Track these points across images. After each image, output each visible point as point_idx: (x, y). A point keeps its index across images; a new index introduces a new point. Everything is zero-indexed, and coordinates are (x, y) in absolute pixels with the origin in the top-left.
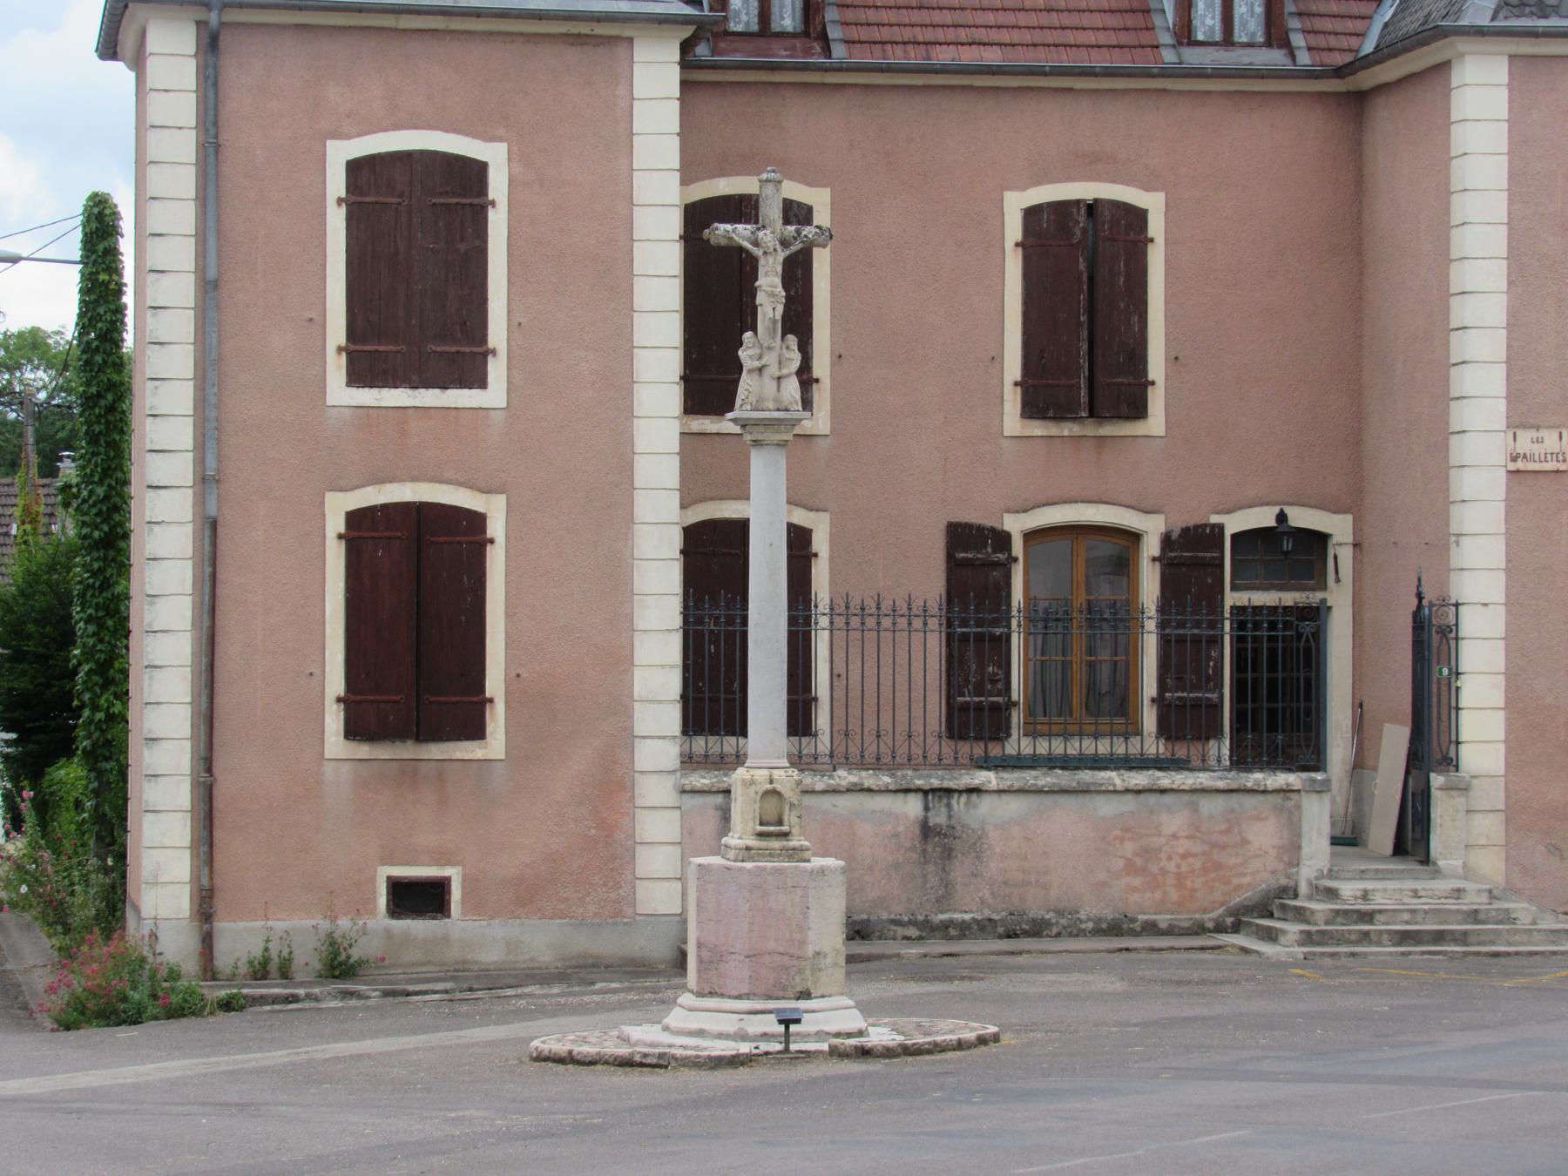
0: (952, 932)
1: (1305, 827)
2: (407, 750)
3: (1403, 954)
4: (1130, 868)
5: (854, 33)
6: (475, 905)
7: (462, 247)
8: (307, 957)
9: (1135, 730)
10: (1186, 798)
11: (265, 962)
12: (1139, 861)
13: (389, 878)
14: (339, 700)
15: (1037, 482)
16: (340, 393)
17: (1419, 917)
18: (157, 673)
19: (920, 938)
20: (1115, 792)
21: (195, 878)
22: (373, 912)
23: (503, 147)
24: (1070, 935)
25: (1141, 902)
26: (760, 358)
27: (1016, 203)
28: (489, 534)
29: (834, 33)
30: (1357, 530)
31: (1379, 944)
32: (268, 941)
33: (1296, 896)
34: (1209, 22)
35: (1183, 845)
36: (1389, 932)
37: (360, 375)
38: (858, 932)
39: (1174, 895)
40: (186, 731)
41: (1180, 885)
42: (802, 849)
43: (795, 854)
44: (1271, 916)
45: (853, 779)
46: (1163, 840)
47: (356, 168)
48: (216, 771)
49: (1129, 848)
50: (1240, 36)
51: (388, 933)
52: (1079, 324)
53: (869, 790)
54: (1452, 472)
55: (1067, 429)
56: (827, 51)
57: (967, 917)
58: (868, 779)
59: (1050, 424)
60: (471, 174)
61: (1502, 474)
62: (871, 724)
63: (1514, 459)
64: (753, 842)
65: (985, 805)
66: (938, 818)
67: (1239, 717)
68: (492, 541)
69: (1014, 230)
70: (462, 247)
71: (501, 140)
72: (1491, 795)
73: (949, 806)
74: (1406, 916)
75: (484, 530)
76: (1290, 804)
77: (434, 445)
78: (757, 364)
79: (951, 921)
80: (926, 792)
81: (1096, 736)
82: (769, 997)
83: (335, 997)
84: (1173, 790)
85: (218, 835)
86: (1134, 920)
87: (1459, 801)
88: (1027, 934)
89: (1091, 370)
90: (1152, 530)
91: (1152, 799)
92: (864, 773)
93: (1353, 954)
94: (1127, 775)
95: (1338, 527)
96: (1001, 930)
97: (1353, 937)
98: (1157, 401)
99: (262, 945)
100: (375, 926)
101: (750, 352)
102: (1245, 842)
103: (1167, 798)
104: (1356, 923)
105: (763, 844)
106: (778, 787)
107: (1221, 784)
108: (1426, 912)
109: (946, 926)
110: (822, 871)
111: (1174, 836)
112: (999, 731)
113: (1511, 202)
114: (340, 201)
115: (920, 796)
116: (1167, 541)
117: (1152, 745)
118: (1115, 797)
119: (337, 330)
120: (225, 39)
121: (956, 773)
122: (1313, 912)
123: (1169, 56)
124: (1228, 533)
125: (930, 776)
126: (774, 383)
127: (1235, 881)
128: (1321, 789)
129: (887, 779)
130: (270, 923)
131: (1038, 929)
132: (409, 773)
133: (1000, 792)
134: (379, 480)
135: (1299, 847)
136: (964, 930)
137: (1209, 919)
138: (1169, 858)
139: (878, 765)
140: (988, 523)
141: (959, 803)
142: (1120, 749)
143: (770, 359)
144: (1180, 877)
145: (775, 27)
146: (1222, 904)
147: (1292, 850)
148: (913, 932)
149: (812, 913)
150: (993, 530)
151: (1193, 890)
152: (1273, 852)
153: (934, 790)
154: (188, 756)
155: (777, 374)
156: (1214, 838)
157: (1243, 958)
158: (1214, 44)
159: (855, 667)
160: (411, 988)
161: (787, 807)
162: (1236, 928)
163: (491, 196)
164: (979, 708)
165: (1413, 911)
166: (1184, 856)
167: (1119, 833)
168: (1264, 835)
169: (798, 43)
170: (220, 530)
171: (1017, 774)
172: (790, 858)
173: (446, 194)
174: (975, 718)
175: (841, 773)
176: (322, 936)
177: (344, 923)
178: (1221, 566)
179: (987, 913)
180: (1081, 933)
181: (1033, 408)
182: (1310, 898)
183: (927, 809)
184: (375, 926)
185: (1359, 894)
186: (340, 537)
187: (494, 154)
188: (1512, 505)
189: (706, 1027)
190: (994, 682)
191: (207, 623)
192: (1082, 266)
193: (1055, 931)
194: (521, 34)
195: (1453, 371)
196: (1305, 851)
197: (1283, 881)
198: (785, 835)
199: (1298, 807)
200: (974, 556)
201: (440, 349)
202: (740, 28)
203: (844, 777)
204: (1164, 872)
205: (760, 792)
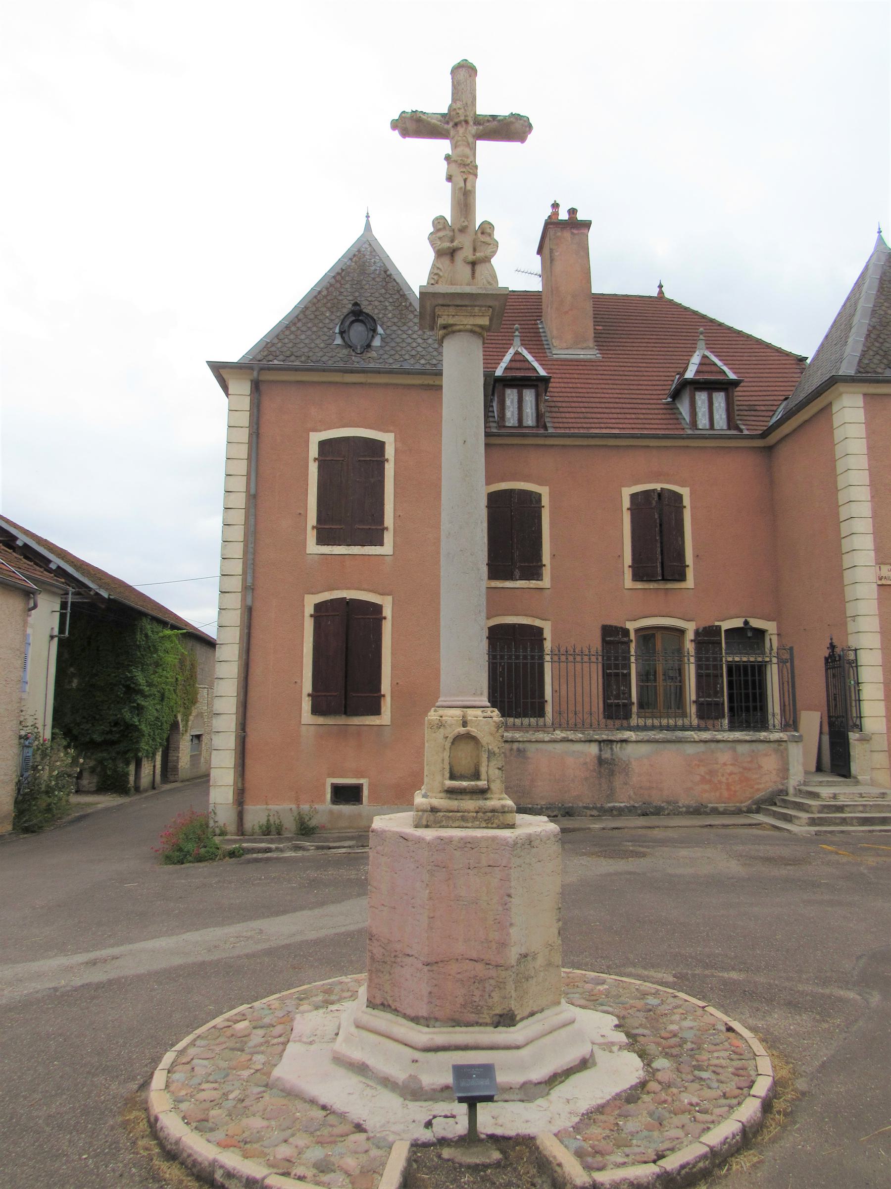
0: (615, 813)
1: (790, 759)
2: (341, 720)
3: (870, 831)
4: (703, 780)
6: (375, 798)
7: (372, 480)
8: (290, 824)
9: (684, 715)
10: (729, 745)
11: (268, 826)
12: (707, 777)
13: (332, 784)
14: (309, 695)
15: (641, 610)
16: (313, 547)
17: (868, 809)
18: (221, 682)
19: (599, 816)
20: (695, 742)
21: (235, 783)
22: (323, 801)
23: (393, 435)
24: (674, 814)
25: (710, 798)
26: (452, 241)
27: (626, 493)
28: (384, 615)
29: (548, 425)
30: (778, 628)
31: (852, 825)
32: (269, 816)
33: (787, 794)
34: (704, 422)
35: (730, 769)
36: (857, 818)
37: (323, 539)
38: (567, 813)
39: (726, 794)
40: (234, 710)
41: (728, 789)
42: (504, 811)
43: (494, 818)
44: (775, 804)
45: (563, 735)
46: (719, 766)
47: (322, 444)
48: (248, 730)
49: (702, 770)
50: (716, 427)
51: (331, 812)
52: (656, 540)
53: (572, 741)
54: (846, 588)
55: (652, 585)
56: (546, 428)
57: (622, 805)
58: (571, 735)
59: (644, 583)
60: (380, 446)
61: (875, 586)
62: (571, 708)
63: (880, 579)
64: (439, 801)
65: (630, 748)
66: (607, 755)
67: (731, 709)
68: (385, 618)
69: (626, 503)
70: (372, 480)
71: (391, 432)
72: (881, 743)
73: (612, 749)
74: (861, 808)
75: (381, 613)
76: (782, 747)
77: (360, 573)
79: (614, 807)
80: (600, 742)
81: (668, 717)
82: (456, 1022)
83: (291, 850)
84: (723, 741)
85: (248, 762)
86: (706, 807)
87: (866, 746)
88: (653, 814)
89: (662, 559)
90: (690, 628)
91: (713, 745)
92: (569, 733)
93: (842, 832)
94: (699, 733)
95: (770, 627)
96: (639, 812)
97: (837, 821)
98: (690, 573)
99: (266, 819)
100: (324, 808)
102: (760, 767)
103: (721, 745)
104: (834, 812)
105: (454, 804)
106: (472, 730)
107: (748, 738)
108: (871, 806)
109: (612, 809)
110: (530, 842)
111: (725, 764)
112: (628, 716)
113: (869, 460)
114: (315, 459)
115: (597, 743)
116: (697, 633)
117: (695, 722)
118: (694, 744)
119: (312, 518)
120: (263, 387)
121: (615, 733)
122: (810, 806)
123: (689, 432)
124: (723, 629)
125: (602, 734)
126: (468, 269)
127: (756, 787)
128: (798, 740)
129: (581, 735)
130: (270, 807)
131: (658, 812)
132: (343, 732)
133: (637, 742)
134: (331, 589)
135: (788, 770)
136: (620, 812)
137: (744, 806)
138: (723, 775)
139: (575, 728)
140: (619, 625)
141: (617, 748)
142: (680, 723)
144: (728, 785)
145: (525, 424)
146: (750, 798)
147: (784, 771)
148: (595, 813)
149: (515, 900)
150: (621, 628)
151: (735, 791)
152: (774, 772)
153: (604, 741)
154: (234, 723)
155: (471, 257)
156: (745, 765)
157: (776, 833)
159: (564, 687)
160: (332, 845)
161: (485, 756)
162: (758, 811)
163: (386, 457)
164: (618, 705)
165: (864, 806)
166: (731, 774)
167: (697, 763)
168: (770, 763)
170: (254, 614)
171: (645, 733)
172: (489, 824)
173: (365, 456)
174: (616, 710)
175: (558, 732)
176: (295, 814)
177: (305, 807)
178: (721, 643)
179: (632, 803)
180: (680, 814)
181: (638, 576)
182: (795, 795)
183: (600, 750)
184: (324, 808)
185: (831, 796)
186: (311, 616)
187: (388, 439)
188: (881, 601)
189: (371, 1062)
190: (624, 694)
191: (244, 657)
192: (656, 516)
193: (666, 812)
194: (402, 385)
195: (843, 540)
196: (791, 771)
197: (781, 787)
198: (483, 792)
199: (786, 749)
200: (613, 636)
201: (361, 527)
202: (510, 425)
203: (559, 734)
204: (720, 782)
205: (451, 736)
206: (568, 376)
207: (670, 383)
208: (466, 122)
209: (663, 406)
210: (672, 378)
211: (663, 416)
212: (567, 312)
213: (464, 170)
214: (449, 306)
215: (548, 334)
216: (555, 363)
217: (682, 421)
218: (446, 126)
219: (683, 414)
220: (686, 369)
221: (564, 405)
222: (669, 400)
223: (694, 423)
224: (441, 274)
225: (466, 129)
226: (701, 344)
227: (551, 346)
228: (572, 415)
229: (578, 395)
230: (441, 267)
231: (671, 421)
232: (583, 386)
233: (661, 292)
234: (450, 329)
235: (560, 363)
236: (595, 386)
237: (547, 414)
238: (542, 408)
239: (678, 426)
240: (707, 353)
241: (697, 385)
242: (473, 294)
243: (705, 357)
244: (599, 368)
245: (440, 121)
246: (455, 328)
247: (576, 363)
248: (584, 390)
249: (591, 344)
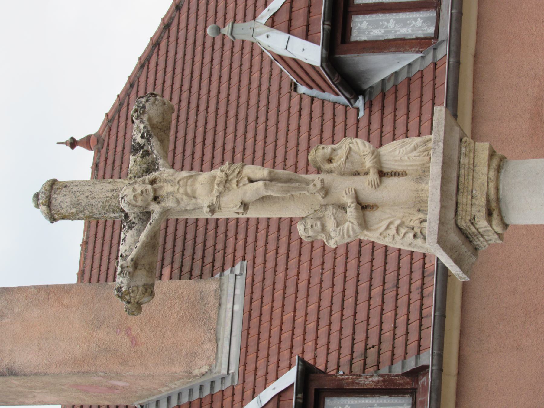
5: (412, 347)
26: (343, 208)
29: (411, 365)
34: (419, 23)
56: (421, 370)
78: (351, 212)
101: (331, 224)
123: (443, 51)
126: (389, 182)
143: (344, 189)
155: (373, 176)
158: (438, 15)
169: (419, 399)
206: (286, 336)
207: (317, 105)
208: (153, 182)
209: (376, 116)
210: (306, 102)
211: (402, 111)
212: (134, 342)
213: (234, 181)
214: (457, 203)
215: (177, 386)
216: (251, 367)
217: (416, 68)
218: (154, 216)
219: (397, 68)
220: (295, 65)
221: (360, 336)
222: (360, 103)
223: (421, 43)
224: (397, 222)
225: (166, 181)
226: (243, 31)
227: (209, 378)
228: (389, 315)
229: (337, 307)
230: (385, 223)
231: (415, 94)
232: (314, 298)
233: (87, 142)
234: (493, 205)
235: (251, 357)
236: (316, 270)
237: (384, 370)
238: (370, 380)
239: (428, 77)
240: (265, 15)
241: (337, 37)
242: (444, 162)
243: (272, 23)
244: (270, 264)
245: (139, 232)
246: (492, 196)
247: (255, 321)
248: (326, 294)
249: (209, 286)
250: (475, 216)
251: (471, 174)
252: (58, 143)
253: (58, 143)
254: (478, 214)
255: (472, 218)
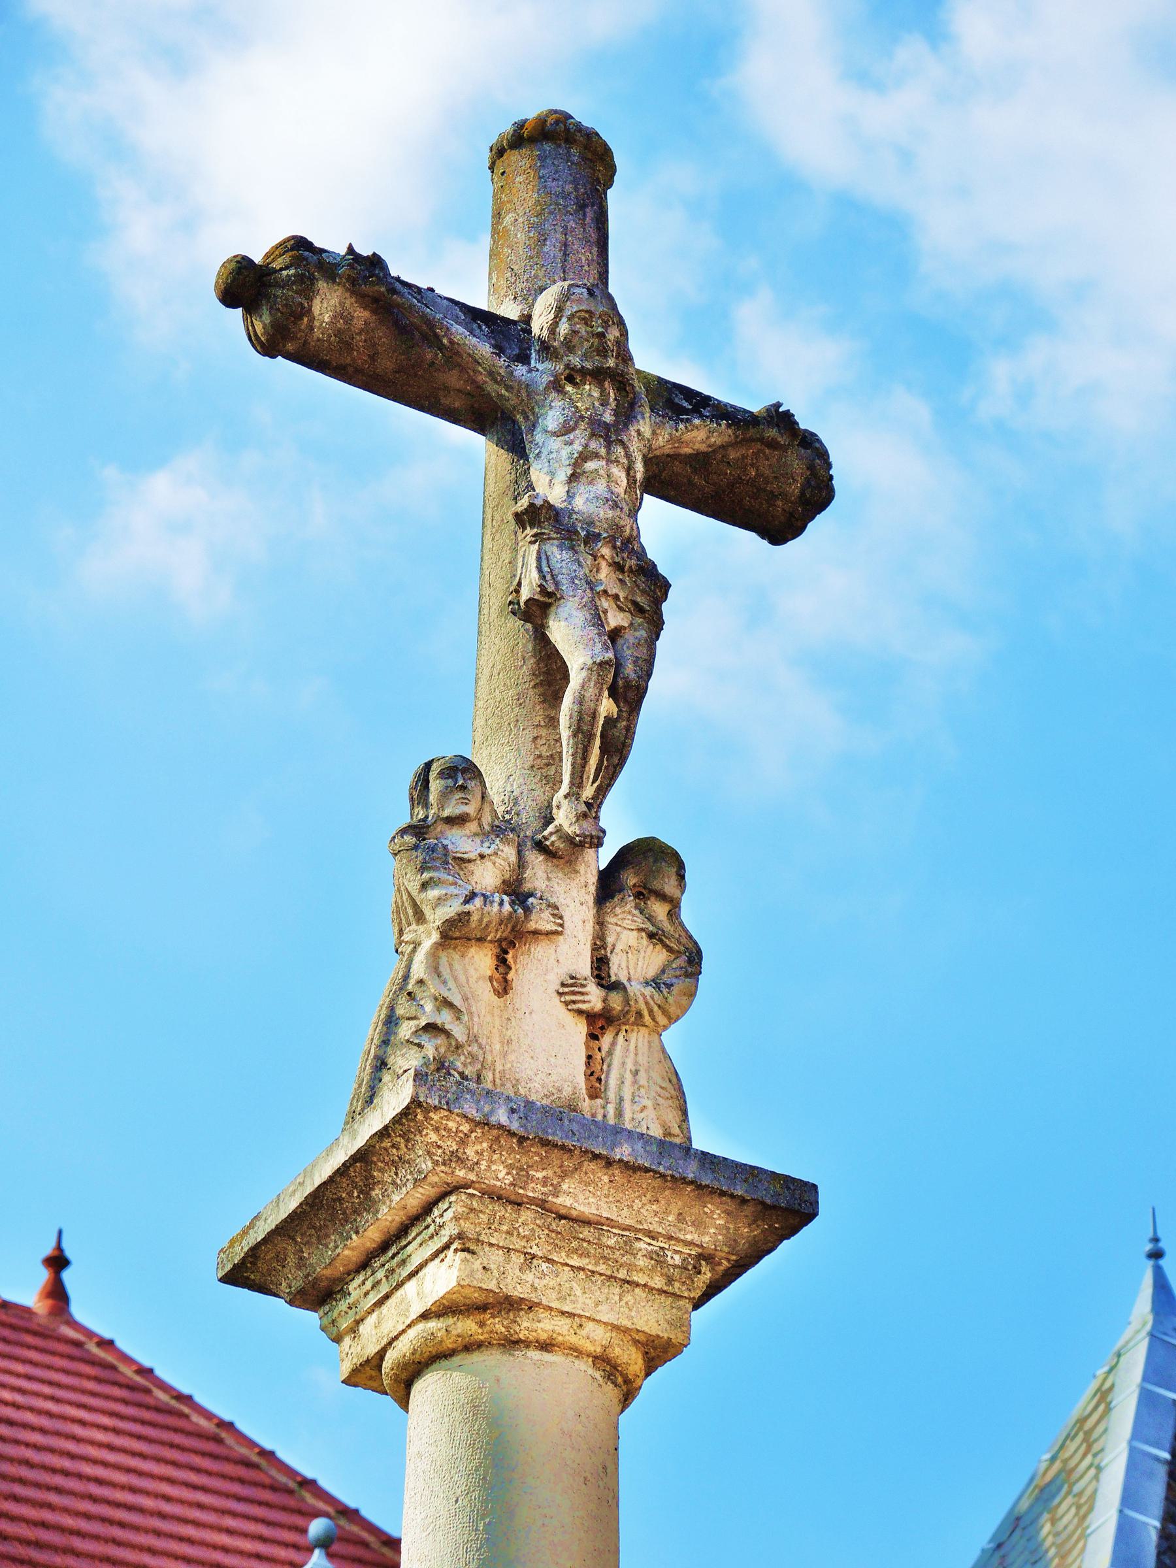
233: (57, 1294)
246: (526, 1326)
250: (473, 1253)
251: (602, 1268)
252: (60, 1233)
253: (60, 1233)
254: (477, 1265)
255: (472, 1247)
